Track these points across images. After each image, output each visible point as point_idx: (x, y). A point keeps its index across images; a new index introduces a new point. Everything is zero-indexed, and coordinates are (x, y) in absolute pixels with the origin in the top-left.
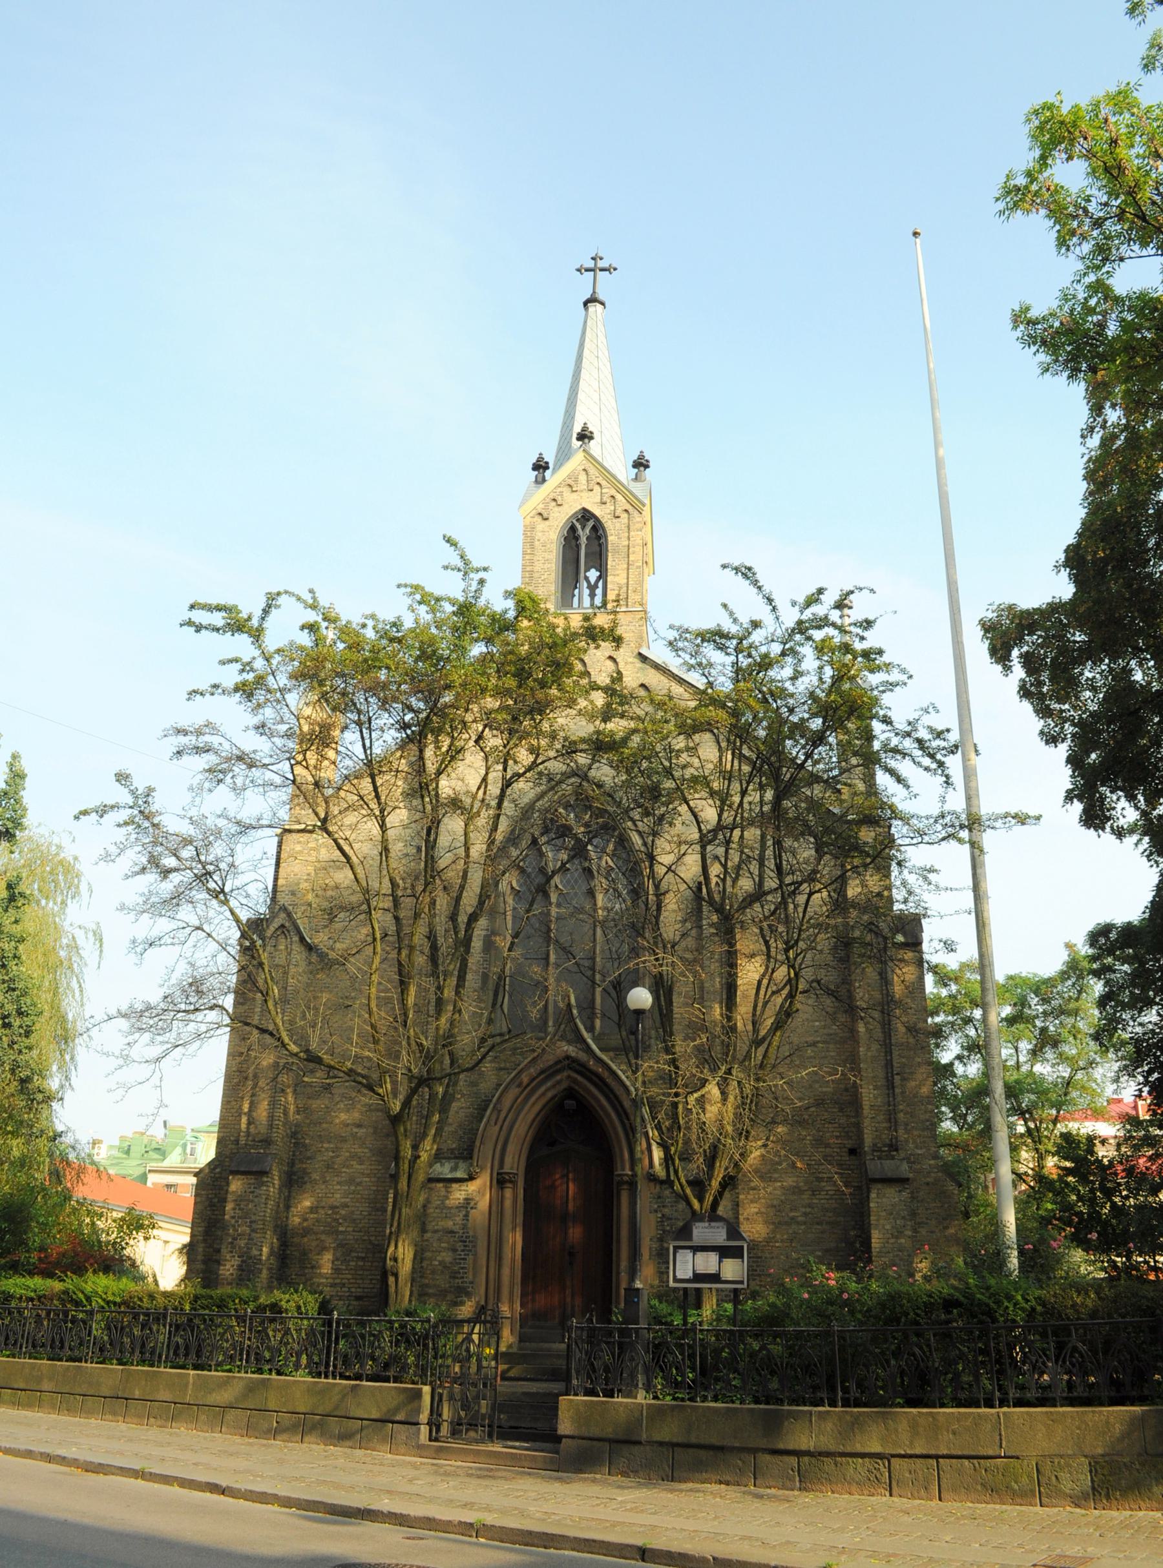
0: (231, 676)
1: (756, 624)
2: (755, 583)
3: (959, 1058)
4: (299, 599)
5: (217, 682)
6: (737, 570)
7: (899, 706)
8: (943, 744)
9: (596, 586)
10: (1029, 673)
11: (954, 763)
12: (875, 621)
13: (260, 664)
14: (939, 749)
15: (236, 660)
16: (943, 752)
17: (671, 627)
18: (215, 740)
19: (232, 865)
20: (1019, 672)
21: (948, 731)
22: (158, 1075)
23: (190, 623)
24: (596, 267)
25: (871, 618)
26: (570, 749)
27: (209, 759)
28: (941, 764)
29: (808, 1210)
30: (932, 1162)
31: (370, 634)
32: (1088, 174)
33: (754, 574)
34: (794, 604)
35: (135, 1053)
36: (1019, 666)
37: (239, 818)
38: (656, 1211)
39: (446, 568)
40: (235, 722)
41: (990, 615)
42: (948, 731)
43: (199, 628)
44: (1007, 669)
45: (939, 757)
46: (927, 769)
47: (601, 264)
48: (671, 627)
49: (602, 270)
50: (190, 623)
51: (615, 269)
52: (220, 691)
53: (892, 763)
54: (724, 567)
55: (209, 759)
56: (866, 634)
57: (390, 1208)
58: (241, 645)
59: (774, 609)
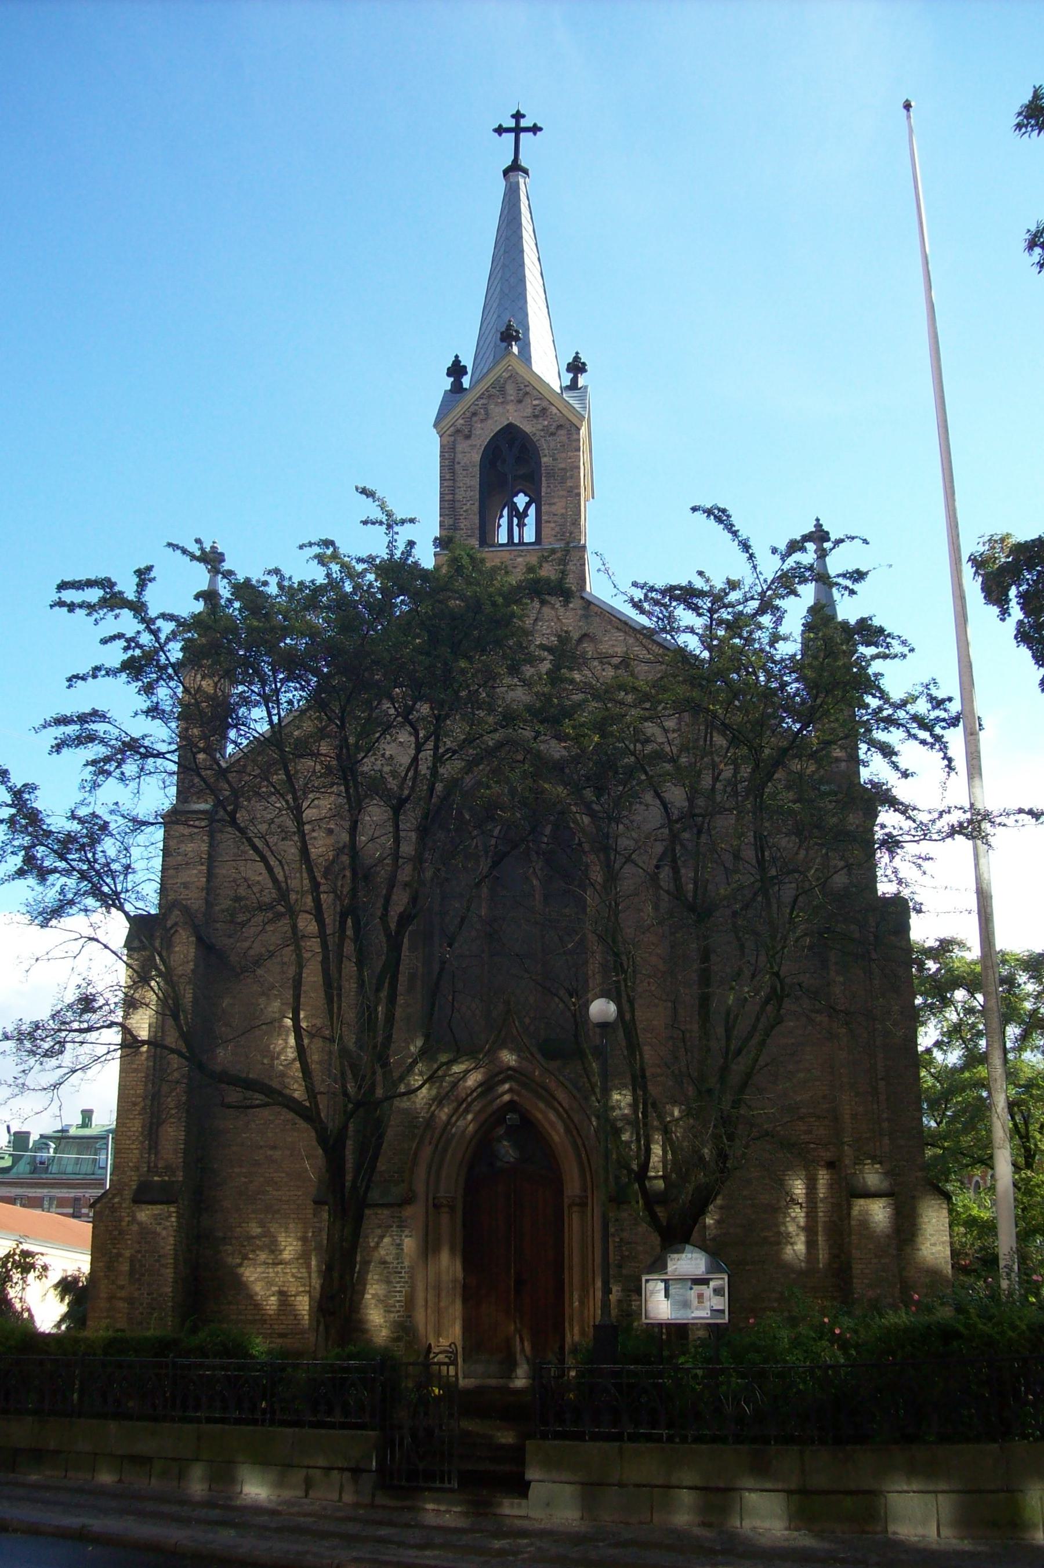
0: (115, 655)
1: (733, 585)
2: (730, 528)
3: (938, 1044)
4: (184, 551)
5: (98, 664)
6: (709, 512)
7: (896, 678)
8: (943, 715)
9: (525, 514)
10: (1027, 615)
11: (955, 737)
12: (867, 573)
13: (146, 639)
14: (938, 720)
15: (120, 636)
16: (943, 724)
17: (635, 584)
18: (100, 728)
19: (128, 867)
20: (1016, 613)
21: (950, 699)
22: (56, 1103)
23: (61, 604)
25: (864, 569)
26: (509, 718)
27: (97, 751)
28: (938, 738)
30: (919, 1174)
31: (273, 589)
33: (729, 516)
34: (774, 551)
35: (30, 1080)
36: (1018, 607)
37: (134, 813)
39: (365, 523)
40: (123, 704)
41: (981, 549)
42: (950, 699)
43: (71, 607)
44: (1004, 613)
45: (938, 730)
46: (923, 742)
47: (524, 123)
48: (635, 584)
49: (527, 130)
50: (61, 604)
52: (103, 672)
53: (880, 735)
54: (694, 509)
55: (97, 751)
56: (856, 587)
58: (127, 622)
59: (751, 557)
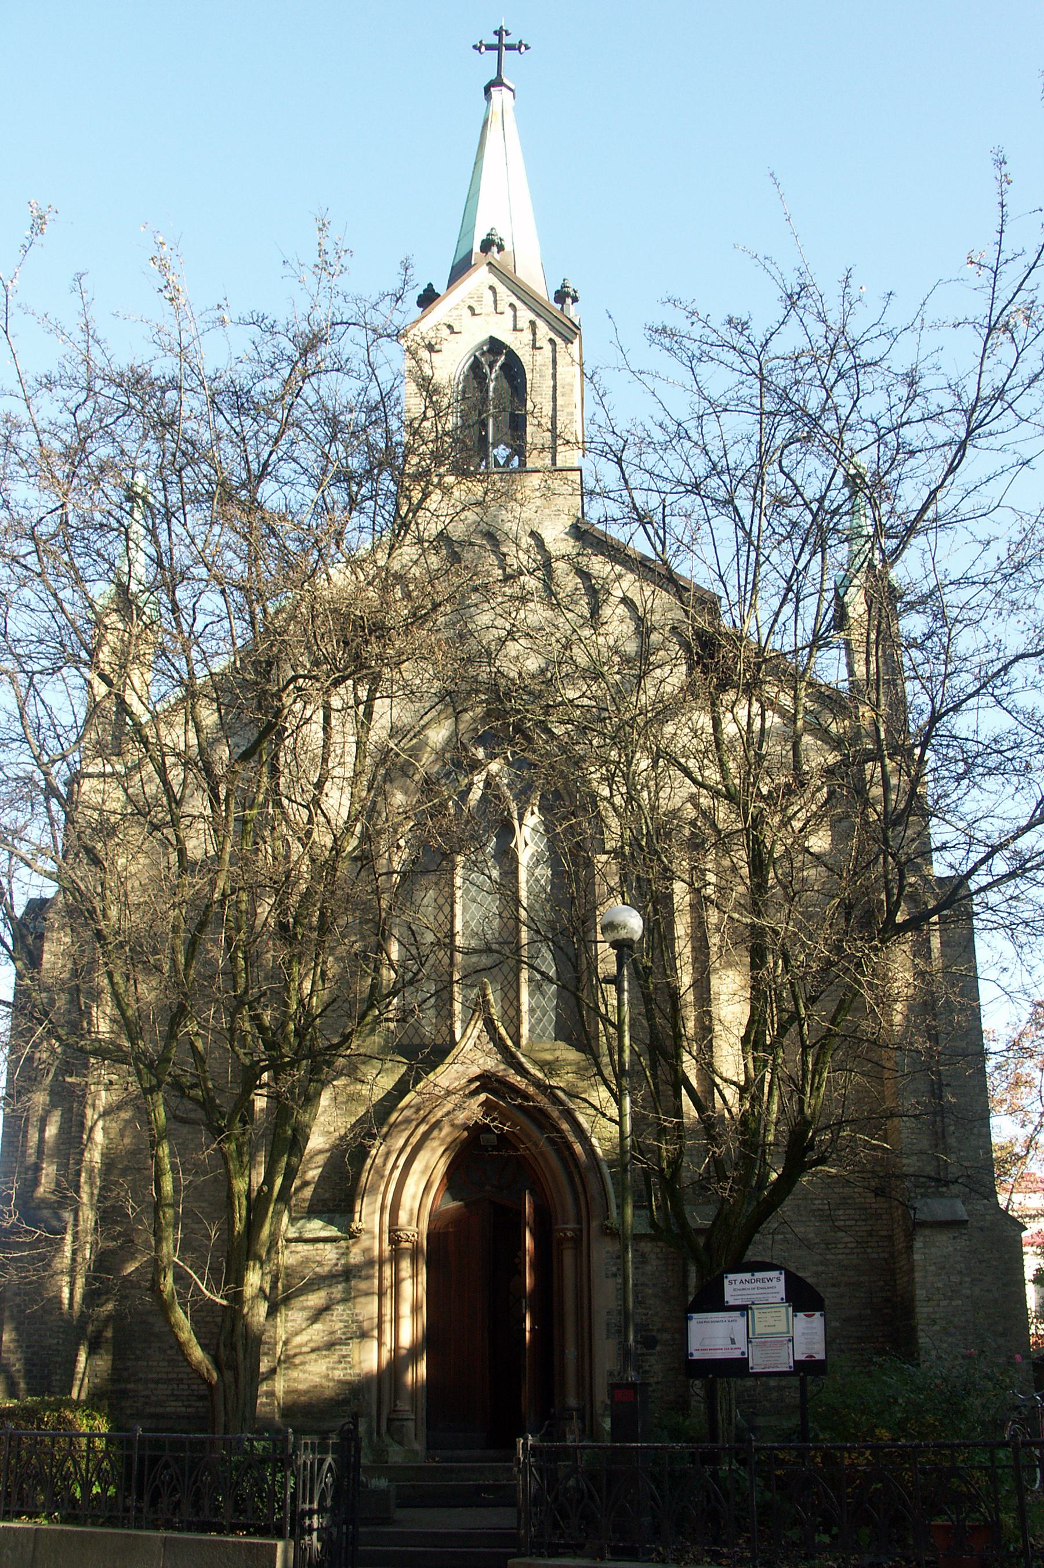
24: (500, 45)
29: (821, 1268)
32: (839, 354)
38: (615, 1275)
47: (506, 40)
49: (510, 48)
51: (527, 48)
57: (765, 1098)
